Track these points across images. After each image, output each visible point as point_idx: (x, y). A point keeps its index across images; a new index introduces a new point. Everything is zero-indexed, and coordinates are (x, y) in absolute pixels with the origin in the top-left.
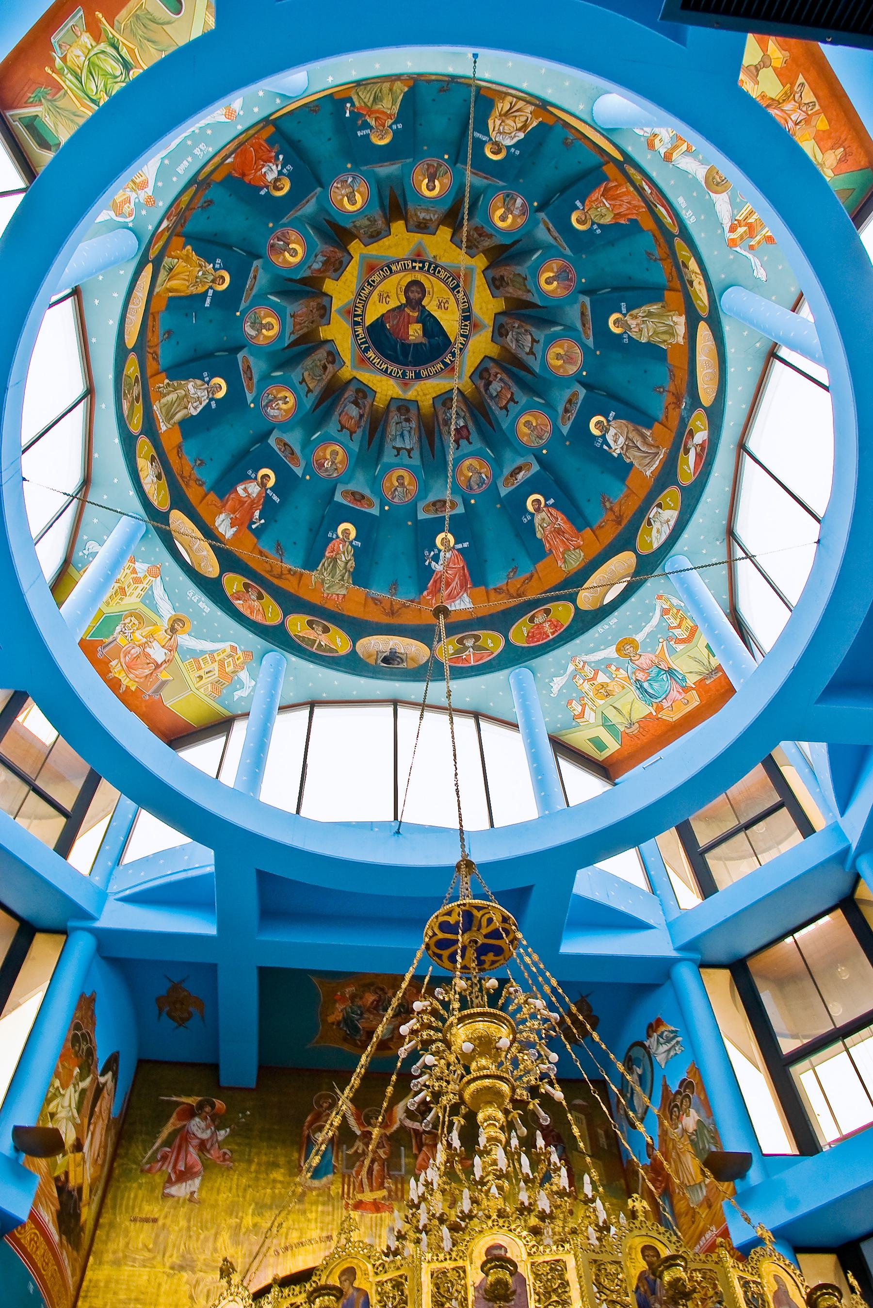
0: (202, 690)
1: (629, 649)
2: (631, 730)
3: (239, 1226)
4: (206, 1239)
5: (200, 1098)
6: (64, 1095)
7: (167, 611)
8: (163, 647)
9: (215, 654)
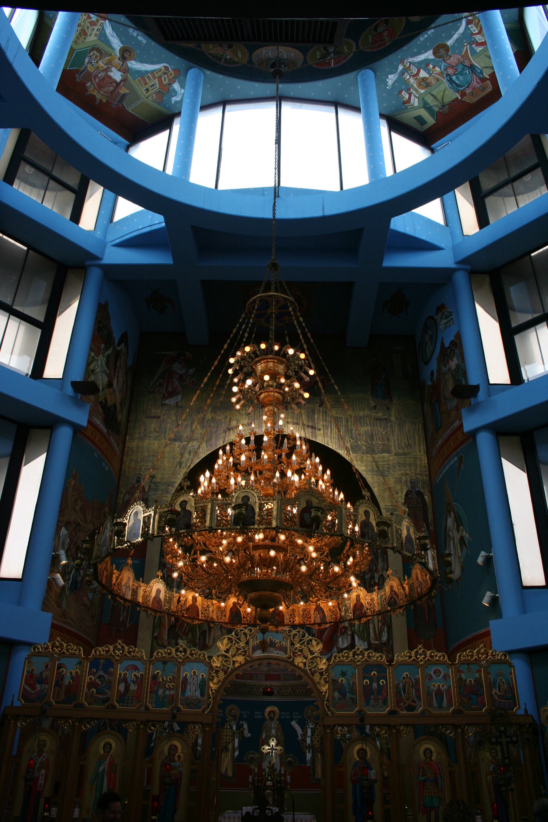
0: (150, 98)
1: (442, 52)
2: (443, 110)
3: (203, 419)
4: (187, 426)
5: (177, 352)
6: (97, 360)
7: (117, 44)
8: (119, 70)
9: (155, 73)
